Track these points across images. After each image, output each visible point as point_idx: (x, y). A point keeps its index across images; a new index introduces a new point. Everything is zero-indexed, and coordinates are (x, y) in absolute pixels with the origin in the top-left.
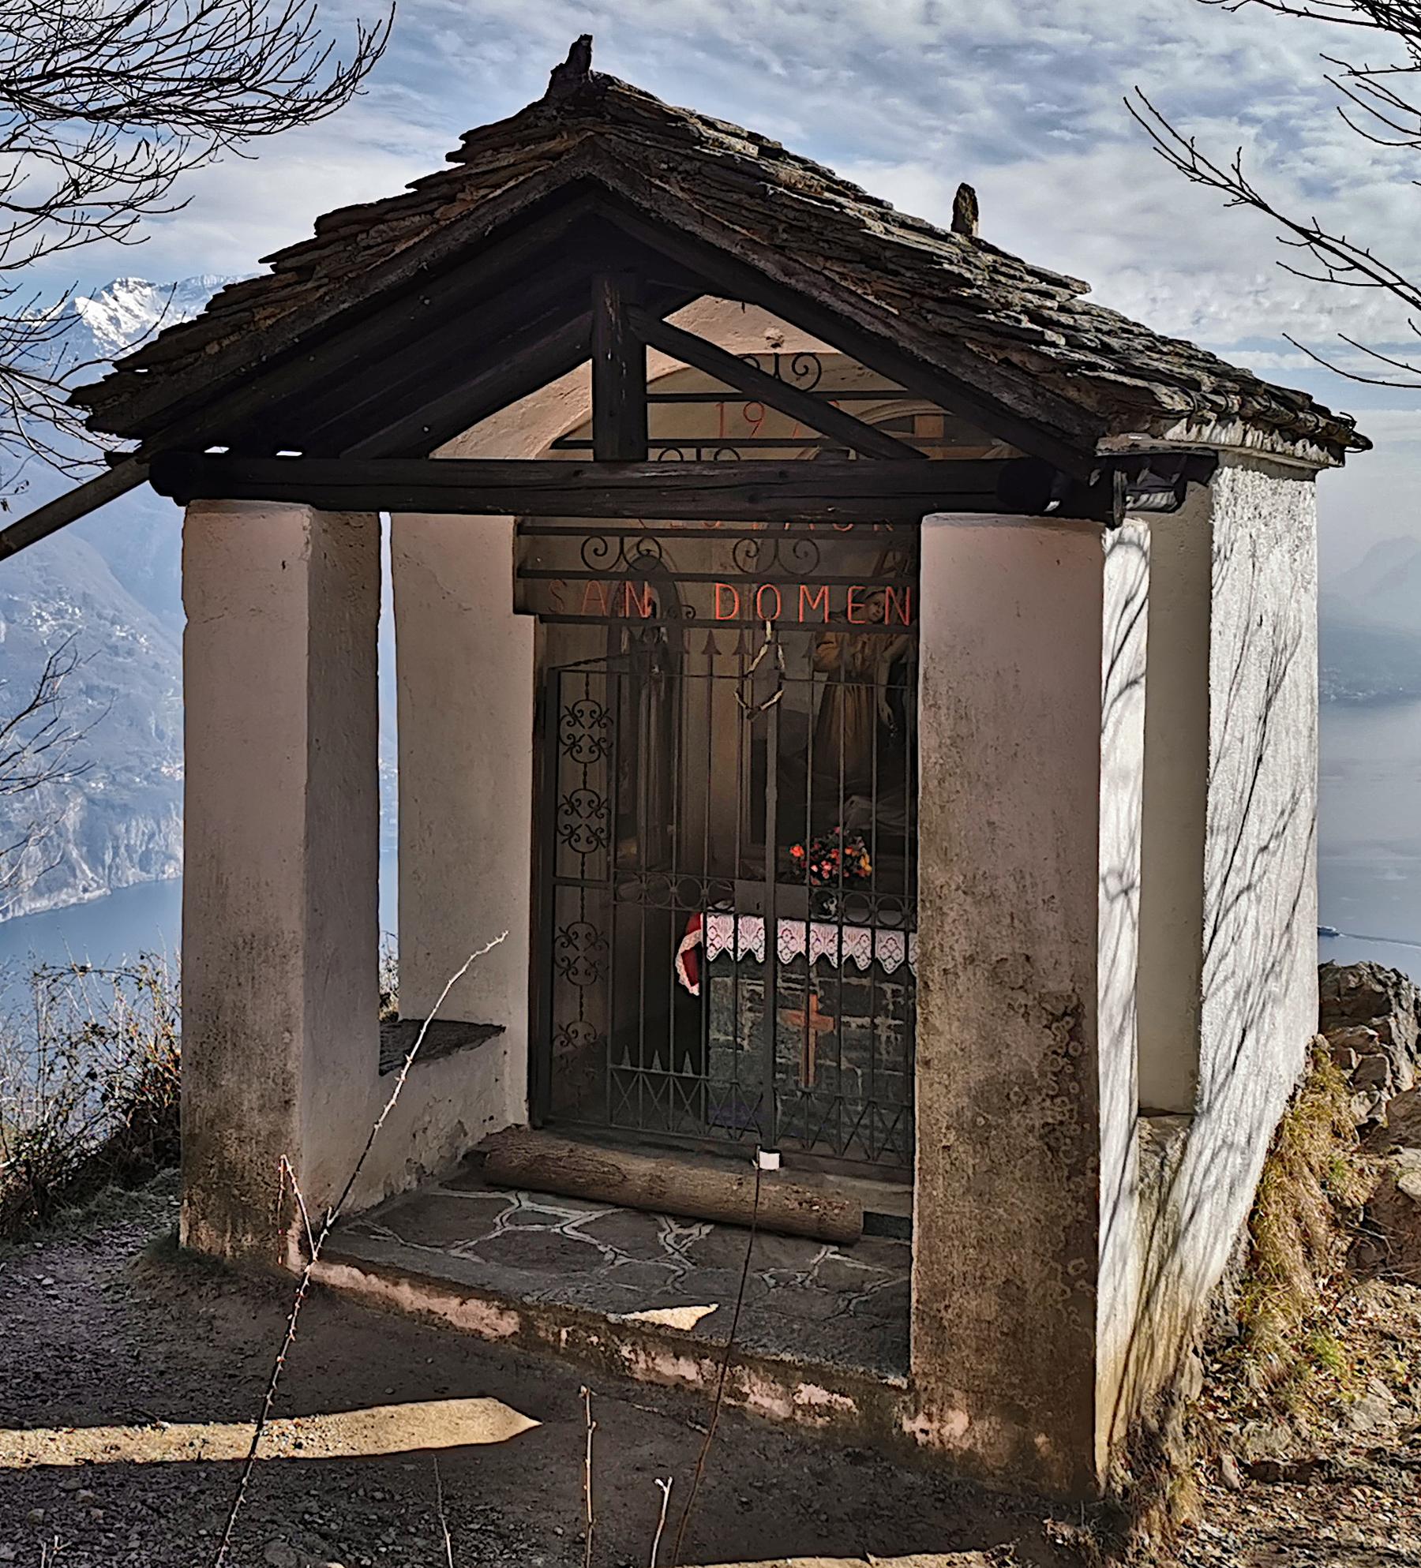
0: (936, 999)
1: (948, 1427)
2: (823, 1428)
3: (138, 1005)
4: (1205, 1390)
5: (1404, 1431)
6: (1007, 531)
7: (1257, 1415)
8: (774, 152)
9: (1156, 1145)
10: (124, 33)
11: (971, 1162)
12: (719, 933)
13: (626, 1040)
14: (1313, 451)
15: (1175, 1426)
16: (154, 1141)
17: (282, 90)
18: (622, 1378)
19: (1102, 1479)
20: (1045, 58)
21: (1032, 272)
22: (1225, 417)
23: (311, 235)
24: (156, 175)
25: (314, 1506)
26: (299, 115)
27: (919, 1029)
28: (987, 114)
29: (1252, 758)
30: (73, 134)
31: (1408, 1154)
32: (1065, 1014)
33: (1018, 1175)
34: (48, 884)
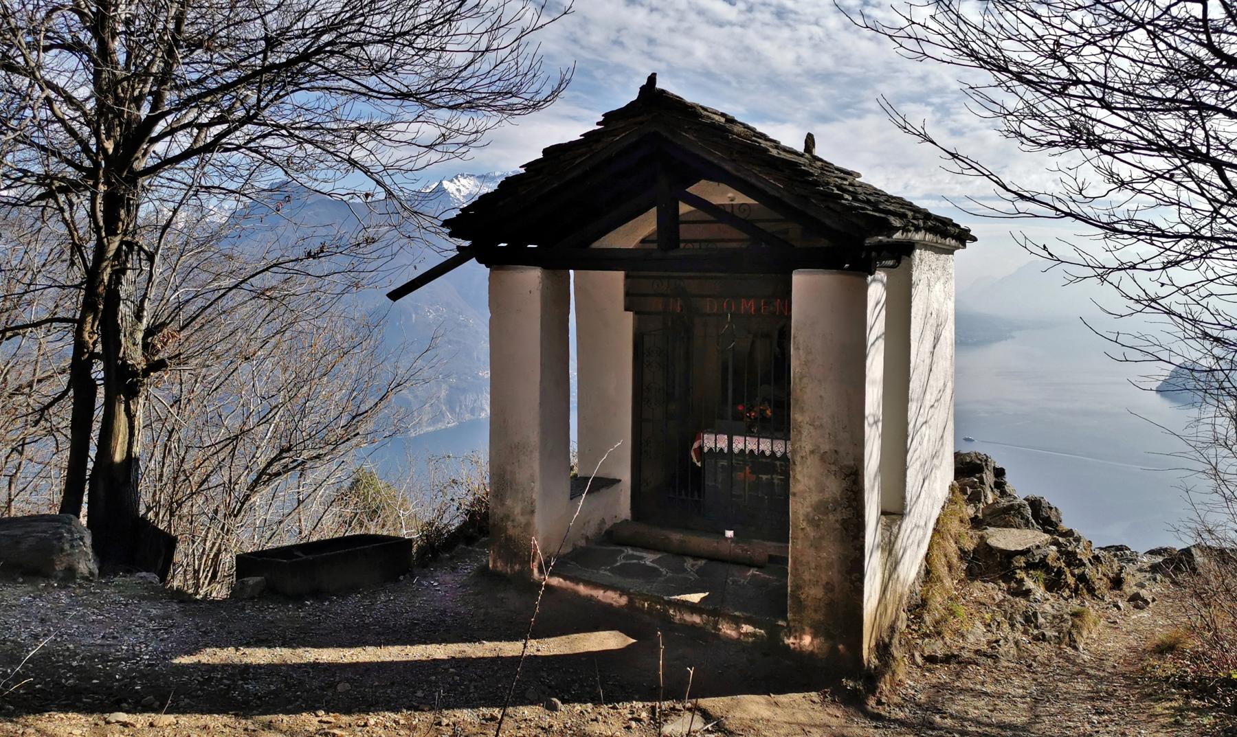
0: (798, 468)
3: (472, 474)
4: (908, 626)
5: (989, 643)
6: (827, 277)
7: (928, 636)
8: (731, 121)
9: (888, 527)
10: (464, 74)
12: (709, 441)
13: (672, 483)
14: (953, 242)
15: (895, 641)
16: (479, 527)
17: (528, 96)
19: (866, 662)
20: (846, 79)
21: (837, 169)
22: (917, 229)
23: (540, 156)
24: (477, 132)
25: (545, 675)
26: (536, 106)
27: (791, 480)
28: (821, 103)
29: (927, 368)
30: (444, 114)
31: (991, 530)
34: (434, 420)
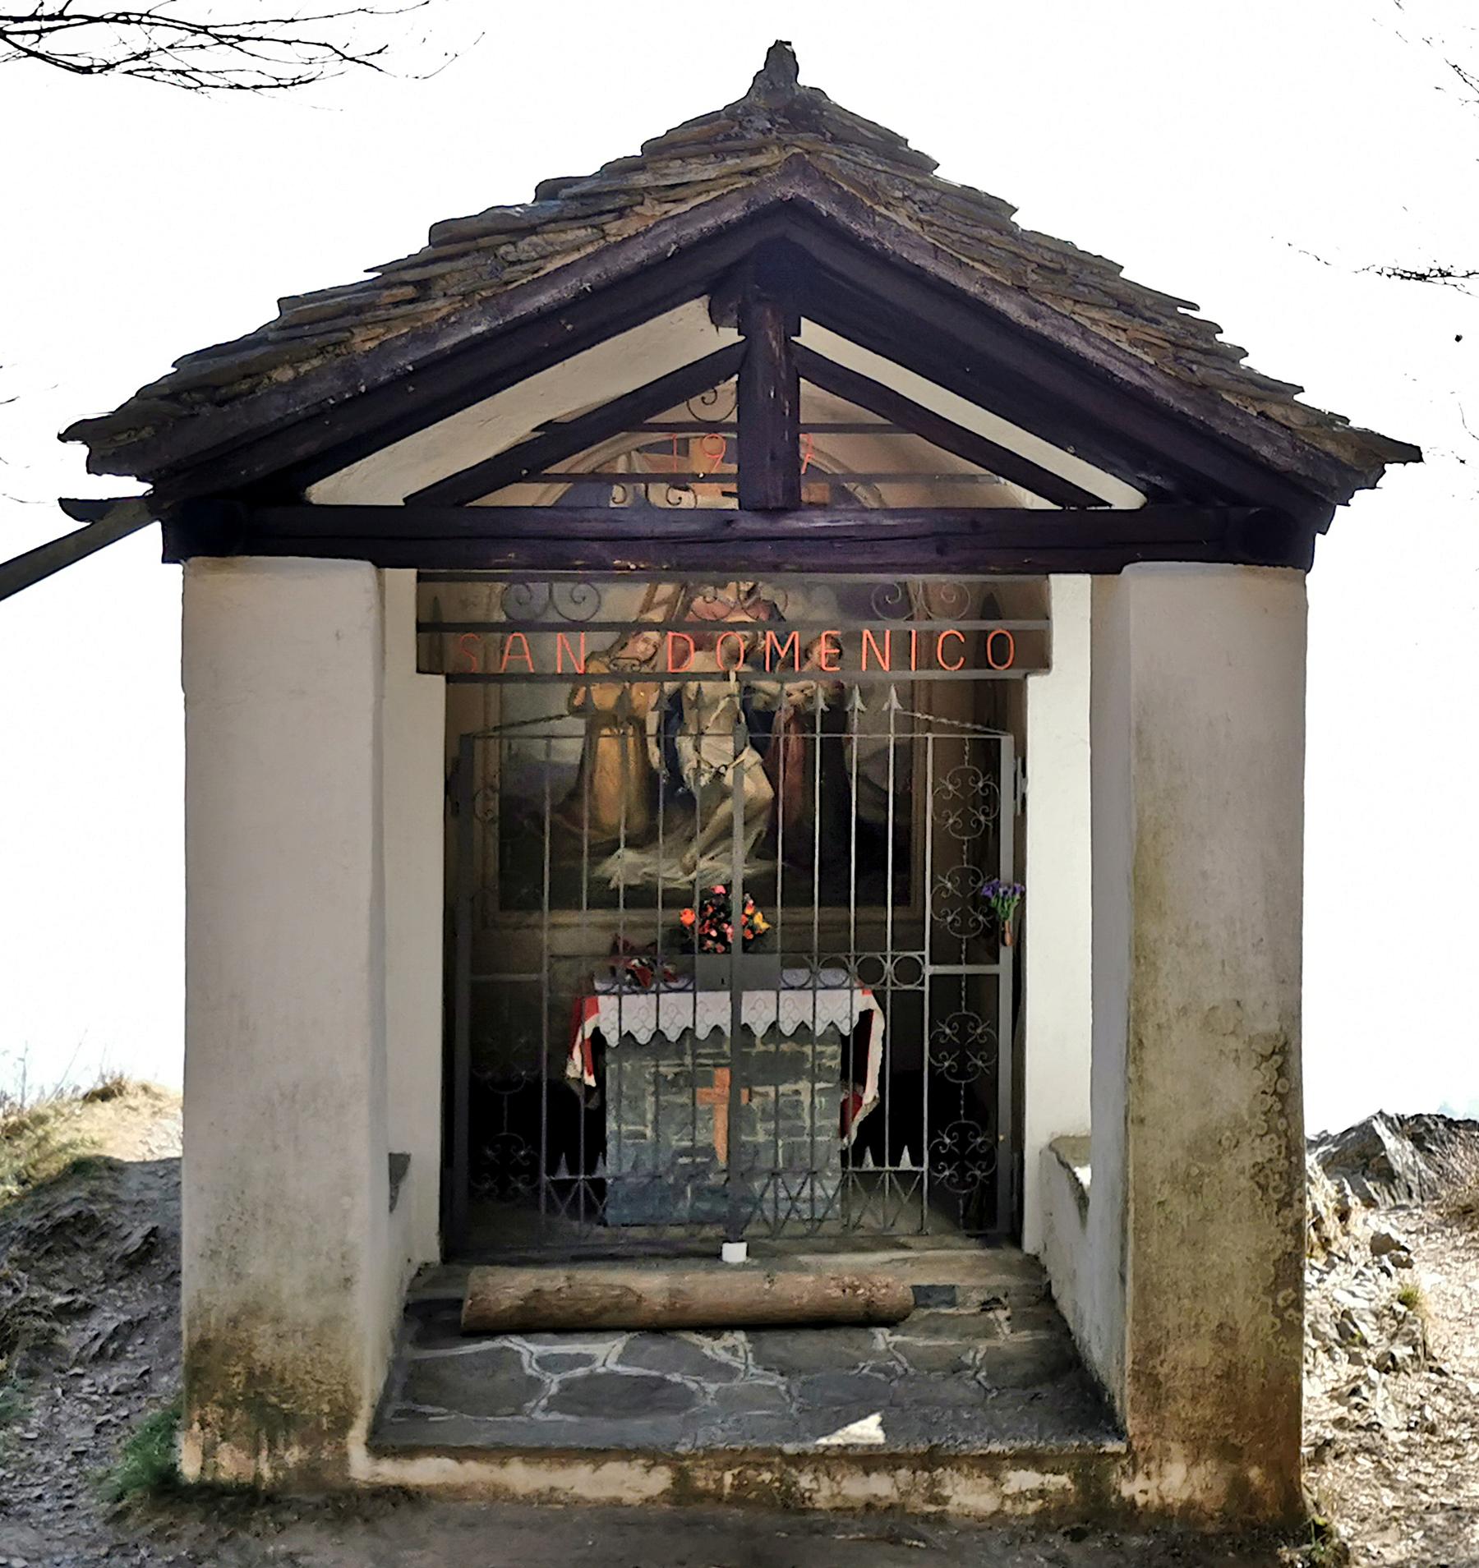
1: (1167, 1481)
2: (1035, 1513)
11: (1185, 1215)
32: (1273, 1053)
33: (1230, 1217)
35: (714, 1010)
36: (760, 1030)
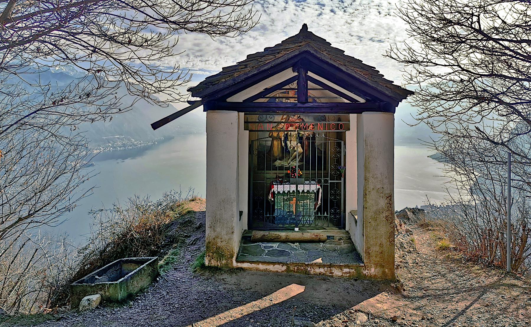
18: (309, 274)
35: (293, 188)
36: (301, 191)
